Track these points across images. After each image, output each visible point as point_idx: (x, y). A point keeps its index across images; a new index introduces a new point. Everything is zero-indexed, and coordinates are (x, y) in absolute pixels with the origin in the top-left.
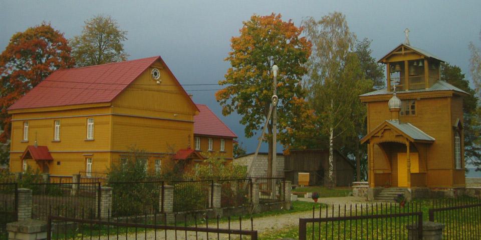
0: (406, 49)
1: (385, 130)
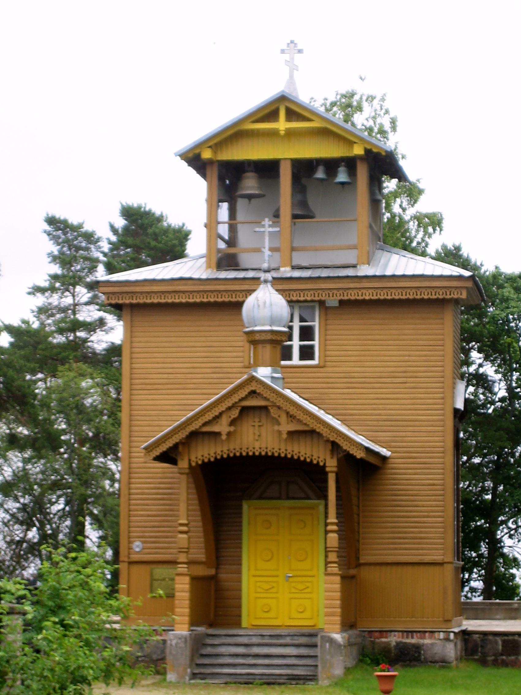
1: (245, 410)
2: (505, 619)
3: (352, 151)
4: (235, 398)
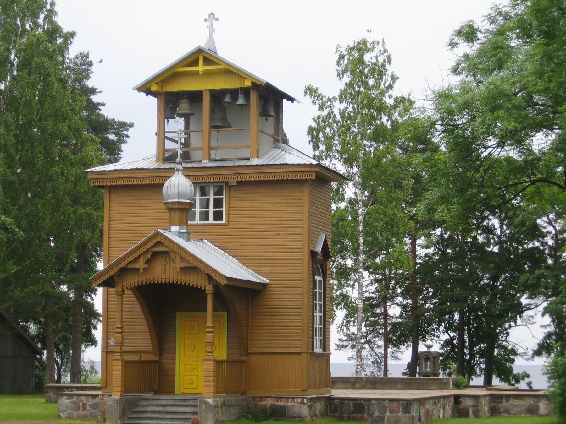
0: (207, 61)
2: (437, 389)
3: (244, 83)
4: (148, 246)
